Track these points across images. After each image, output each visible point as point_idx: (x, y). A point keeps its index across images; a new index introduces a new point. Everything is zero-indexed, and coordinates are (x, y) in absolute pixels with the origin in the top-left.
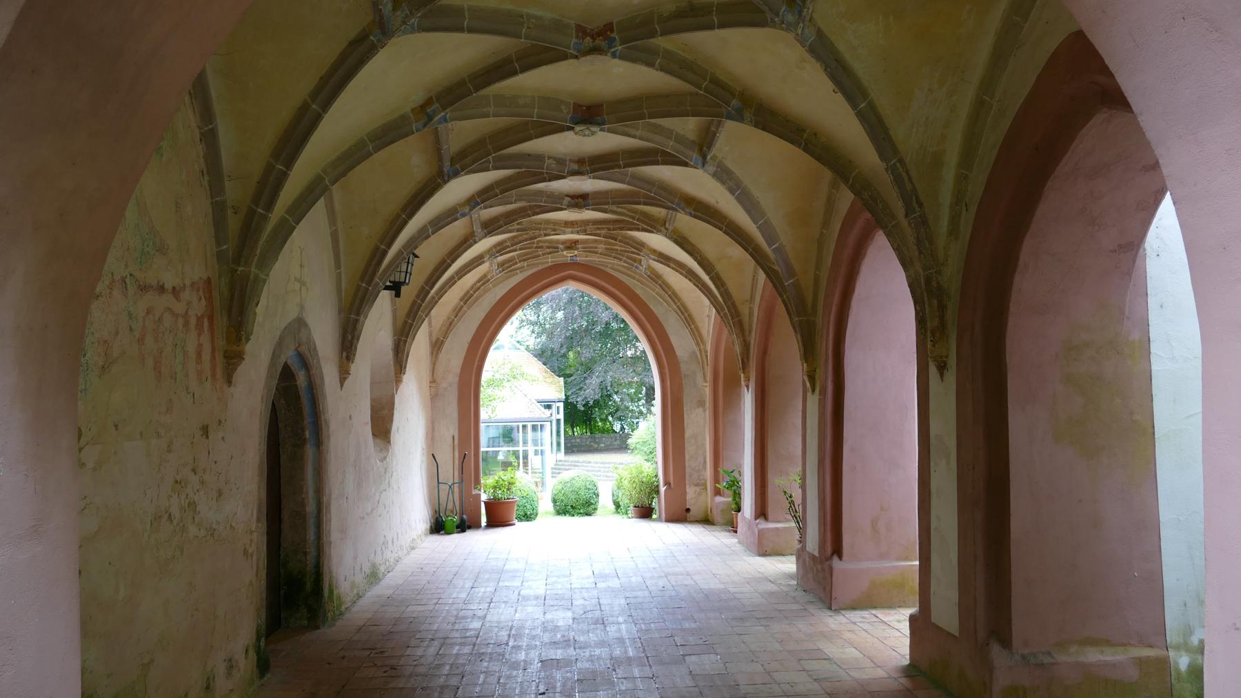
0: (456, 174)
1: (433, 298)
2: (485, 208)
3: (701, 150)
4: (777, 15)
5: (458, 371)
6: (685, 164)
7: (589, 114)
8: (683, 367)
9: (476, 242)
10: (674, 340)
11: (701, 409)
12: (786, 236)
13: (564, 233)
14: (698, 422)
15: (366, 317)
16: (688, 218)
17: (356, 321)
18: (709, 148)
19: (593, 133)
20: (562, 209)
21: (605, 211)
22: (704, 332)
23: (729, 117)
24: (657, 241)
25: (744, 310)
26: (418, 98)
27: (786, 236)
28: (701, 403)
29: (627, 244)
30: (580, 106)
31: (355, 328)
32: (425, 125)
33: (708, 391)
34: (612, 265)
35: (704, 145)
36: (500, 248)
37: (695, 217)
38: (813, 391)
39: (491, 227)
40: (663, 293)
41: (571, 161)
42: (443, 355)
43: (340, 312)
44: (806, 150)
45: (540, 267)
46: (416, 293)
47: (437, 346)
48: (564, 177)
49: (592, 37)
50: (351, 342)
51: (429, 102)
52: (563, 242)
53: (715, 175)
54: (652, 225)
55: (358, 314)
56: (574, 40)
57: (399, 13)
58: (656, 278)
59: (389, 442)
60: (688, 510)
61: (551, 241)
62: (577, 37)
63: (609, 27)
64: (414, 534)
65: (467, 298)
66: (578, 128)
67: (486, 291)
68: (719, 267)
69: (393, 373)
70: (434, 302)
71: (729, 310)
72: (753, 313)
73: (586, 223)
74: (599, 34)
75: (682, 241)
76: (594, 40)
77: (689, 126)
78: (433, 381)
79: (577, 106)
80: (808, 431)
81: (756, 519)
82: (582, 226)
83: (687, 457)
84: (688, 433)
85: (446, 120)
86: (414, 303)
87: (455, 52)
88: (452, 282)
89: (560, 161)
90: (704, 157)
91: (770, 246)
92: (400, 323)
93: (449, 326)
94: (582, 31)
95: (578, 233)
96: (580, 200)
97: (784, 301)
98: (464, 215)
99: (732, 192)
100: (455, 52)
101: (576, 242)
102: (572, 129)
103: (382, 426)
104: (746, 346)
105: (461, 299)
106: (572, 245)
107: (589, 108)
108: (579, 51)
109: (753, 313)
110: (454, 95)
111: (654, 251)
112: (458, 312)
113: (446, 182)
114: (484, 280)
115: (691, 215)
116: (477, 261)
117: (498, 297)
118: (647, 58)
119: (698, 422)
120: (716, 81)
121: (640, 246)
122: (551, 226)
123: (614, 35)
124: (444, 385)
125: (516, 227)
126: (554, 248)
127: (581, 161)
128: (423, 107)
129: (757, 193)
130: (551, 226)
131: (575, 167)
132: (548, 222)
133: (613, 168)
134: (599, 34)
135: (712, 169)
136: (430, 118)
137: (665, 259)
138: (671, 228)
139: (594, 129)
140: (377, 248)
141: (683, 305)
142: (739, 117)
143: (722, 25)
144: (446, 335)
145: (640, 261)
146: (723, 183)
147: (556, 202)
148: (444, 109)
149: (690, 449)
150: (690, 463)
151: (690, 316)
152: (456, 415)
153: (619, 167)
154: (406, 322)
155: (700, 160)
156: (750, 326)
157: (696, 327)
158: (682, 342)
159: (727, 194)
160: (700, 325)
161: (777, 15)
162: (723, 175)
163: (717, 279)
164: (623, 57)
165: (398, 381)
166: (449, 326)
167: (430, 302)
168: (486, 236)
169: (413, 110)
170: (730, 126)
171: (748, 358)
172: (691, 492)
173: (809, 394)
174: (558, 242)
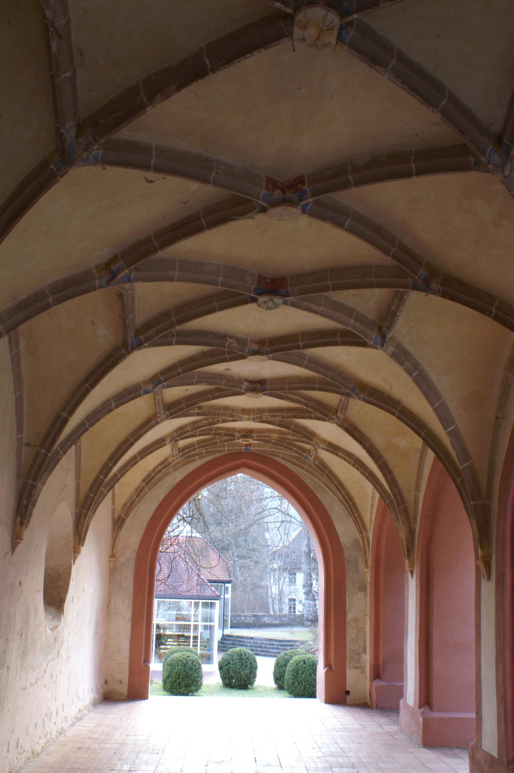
0: (139, 345)
1: (116, 475)
2: (168, 387)
3: (380, 328)
4: (484, 154)
5: (137, 547)
6: (364, 345)
7: (273, 287)
8: (346, 552)
9: (158, 423)
10: (339, 527)
11: (362, 594)
12: (461, 420)
13: (241, 419)
14: (359, 606)
15: (43, 484)
16: (361, 403)
17: (33, 487)
18: (389, 328)
19: (276, 306)
20: (240, 394)
21: (281, 397)
22: (367, 520)
23: (416, 288)
24: (327, 430)
25: (409, 497)
26: (103, 254)
27: (461, 420)
28: (363, 589)
29: (299, 433)
30: (265, 278)
31: (30, 495)
32: (108, 283)
33: (369, 577)
34: (282, 456)
35: (388, 317)
36: (181, 433)
37: (369, 402)
38: (489, 578)
39: (174, 409)
40: (329, 483)
41: (252, 341)
42: (123, 533)
43: (19, 475)
44: (497, 318)
45: (217, 455)
46: (99, 468)
47: (118, 523)
48: (243, 357)
49: (283, 191)
50: (26, 507)
51: (114, 259)
52: (240, 431)
53: (393, 356)
54: (324, 412)
55: (35, 479)
56: (264, 191)
57: (82, 140)
58: (323, 468)
59: (62, 611)
60: (348, 693)
61: (227, 429)
62: (267, 188)
63: (300, 180)
64: (71, 711)
65: (149, 481)
66: (262, 299)
67: (167, 474)
68: (387, 456)
69: (72, 545)
70: (116, 479)
71: (394, 499)
72: (419, 498)
73: (262, 411)
74: (289, 187)
75: (352, 430)
76: (284, 192)
77: (369, 300)
78: (113, 556)
79: (261, 278)
80: (483, 620)
81: (420, 707)
82: (258, 414)
83: (348, 639)
84: (349, 617)
85: (130, 280)
86: (97, 478)
87: (142, 200)
88: (133, 461)
89: (242, 341)
90: (384, 337)
91: (445, 428)
92: (82, 496)
93: (130, 505)
94: (272, 183)
95: (254, 420)
96: (258, 386)
97: (457, 486)
98: (147, 392)
99: (409, 372)
100: (142, 200)
101: (251, 431)
102: (254, 300)
103: (55, 597)
104: (411, 532)
105: (143, 481)
106: (247, 434)
107: (273, 281)
108: (268, 202)
109: (419, 498)
110: (138, 255)
111: (324, 441)
112: (140, 492)
113: (129, 353)
114: (165, 464)
115: (364, 400)
116: (159, 443)
117: (177, 481)
118: (335, 216)
119: (359, 606)
120: (403, 249)
121: (309, 435)
122: (229, 412)
123: (306, 187)
124: (123, 559)
125: (197, 411)
126: (231, 434)
127: (261, 342)
128: (108, 265)
129: (434, 377)
130: (229, 412)
131: (256, 347)
132: (226, 408)
133: (293, 348)
134: (289, 187)
135: (391, 349)
136: (114, 275)
137: (334, 449)
138: (342, 417)
139: (278, 300)
140: (58, 416)
141: (348, 494)
142: (425, 287)
143: (420, 172)
144: (127, 514)
145: (310, 451)
146: (401, 364)
147: (233, 386)
148: (128, 266)
149: (351, 633)
150: (350, 646)
151: (354, 505)
152: (131, 589)
153: (298, 347)
154: (87, 496)
155: (380, 339)
156: (416, 513)
157: (360, 516)
158: (345, 529)
159: (405, 375)
160: (362, 513)
161: (484, 154)
162: (402, 356)
163: (384, 467)
164: (312, 214)
165: (76, 552)
166: (130, 505)
167: (112, 479)
168: (167, 418)
169: (97, 267)
170: (414, 298)
171: (413, 546)
172: (351, 675)
173: (483, 581)
174: (234, 430)
